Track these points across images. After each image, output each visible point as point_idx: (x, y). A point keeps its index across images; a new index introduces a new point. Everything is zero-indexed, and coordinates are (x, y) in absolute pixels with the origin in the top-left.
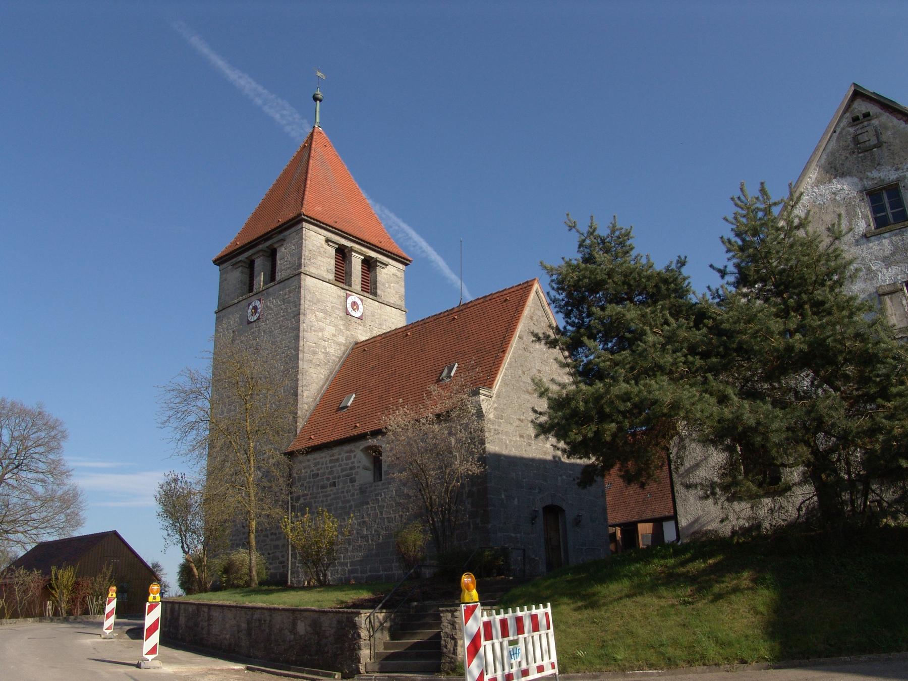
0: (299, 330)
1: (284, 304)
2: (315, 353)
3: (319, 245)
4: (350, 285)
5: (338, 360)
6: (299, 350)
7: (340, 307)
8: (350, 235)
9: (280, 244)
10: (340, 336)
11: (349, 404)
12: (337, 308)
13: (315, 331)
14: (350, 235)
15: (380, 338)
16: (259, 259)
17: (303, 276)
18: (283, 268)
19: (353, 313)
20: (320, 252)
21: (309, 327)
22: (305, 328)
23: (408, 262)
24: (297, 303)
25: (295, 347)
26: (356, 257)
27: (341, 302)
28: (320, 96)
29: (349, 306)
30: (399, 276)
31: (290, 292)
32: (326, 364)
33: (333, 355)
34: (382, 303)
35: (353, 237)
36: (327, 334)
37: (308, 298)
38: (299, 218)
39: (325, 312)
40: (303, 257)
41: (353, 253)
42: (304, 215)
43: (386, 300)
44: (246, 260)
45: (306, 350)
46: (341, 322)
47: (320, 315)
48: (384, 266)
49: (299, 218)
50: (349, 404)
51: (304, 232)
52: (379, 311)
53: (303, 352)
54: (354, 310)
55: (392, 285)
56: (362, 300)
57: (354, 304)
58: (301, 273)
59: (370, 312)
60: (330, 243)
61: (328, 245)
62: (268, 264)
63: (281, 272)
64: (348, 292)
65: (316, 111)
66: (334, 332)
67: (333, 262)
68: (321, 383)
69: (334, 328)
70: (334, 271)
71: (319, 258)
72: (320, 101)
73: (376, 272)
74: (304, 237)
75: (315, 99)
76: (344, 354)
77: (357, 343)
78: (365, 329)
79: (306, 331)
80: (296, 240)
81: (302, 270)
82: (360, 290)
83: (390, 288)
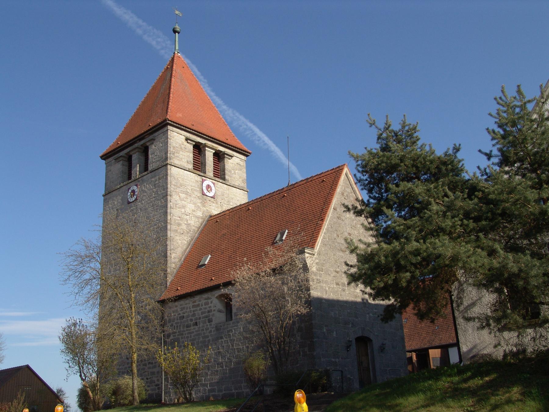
1: (155, 188)
2: (179, 225)
3: (181, 142)
4: (205, 173)
5: (197, 229)
6: (167, 223)
7: (198, 189)
8: (204, 135)
10: (198, 212)
11: (206, 263)
13: (179, 208)
14: (204, 135)
15: (228, 212)
16: (135, 155)
17: (169, 167)
18: (154, 161)
21: (175, 205)
22: (172, 205)
23: (248, 154)
27: (198, 186)
30: (242, 165)
31: (159, 179)
32: (188, 233)
33: (193, 226)
35: (206, 136)
36: (188, 210)
37: (173, 183)
39: (187, 193)
40: (169, 152)
41: (207, 148)
42: (169, 120)
43: (233, 183)
45: (173, 222)
46: (199, 201)
47: (183, 196)
48: (230, 158)
50: (206, 263)
51: (169, 133)
52: (227, 192)
55: (237, 172)
56: (214, 184)
58: (168, 164)
60: (189, 141)
61: (188, 142)
62: (143, 159)
64: (204, 178)
65: (175, 41)
66: (193, 208)
68: (185, 247)
70: (192, 162)
71: (181, 153)
72: (179, 33)
73: (224, 162)
75: (175, 31)
76: (201, 224)
77: (211, 216)
78: (217, 205)
79: (172, 208)
80: (163, 139)
81: (169, 162)
83: (235, 174)
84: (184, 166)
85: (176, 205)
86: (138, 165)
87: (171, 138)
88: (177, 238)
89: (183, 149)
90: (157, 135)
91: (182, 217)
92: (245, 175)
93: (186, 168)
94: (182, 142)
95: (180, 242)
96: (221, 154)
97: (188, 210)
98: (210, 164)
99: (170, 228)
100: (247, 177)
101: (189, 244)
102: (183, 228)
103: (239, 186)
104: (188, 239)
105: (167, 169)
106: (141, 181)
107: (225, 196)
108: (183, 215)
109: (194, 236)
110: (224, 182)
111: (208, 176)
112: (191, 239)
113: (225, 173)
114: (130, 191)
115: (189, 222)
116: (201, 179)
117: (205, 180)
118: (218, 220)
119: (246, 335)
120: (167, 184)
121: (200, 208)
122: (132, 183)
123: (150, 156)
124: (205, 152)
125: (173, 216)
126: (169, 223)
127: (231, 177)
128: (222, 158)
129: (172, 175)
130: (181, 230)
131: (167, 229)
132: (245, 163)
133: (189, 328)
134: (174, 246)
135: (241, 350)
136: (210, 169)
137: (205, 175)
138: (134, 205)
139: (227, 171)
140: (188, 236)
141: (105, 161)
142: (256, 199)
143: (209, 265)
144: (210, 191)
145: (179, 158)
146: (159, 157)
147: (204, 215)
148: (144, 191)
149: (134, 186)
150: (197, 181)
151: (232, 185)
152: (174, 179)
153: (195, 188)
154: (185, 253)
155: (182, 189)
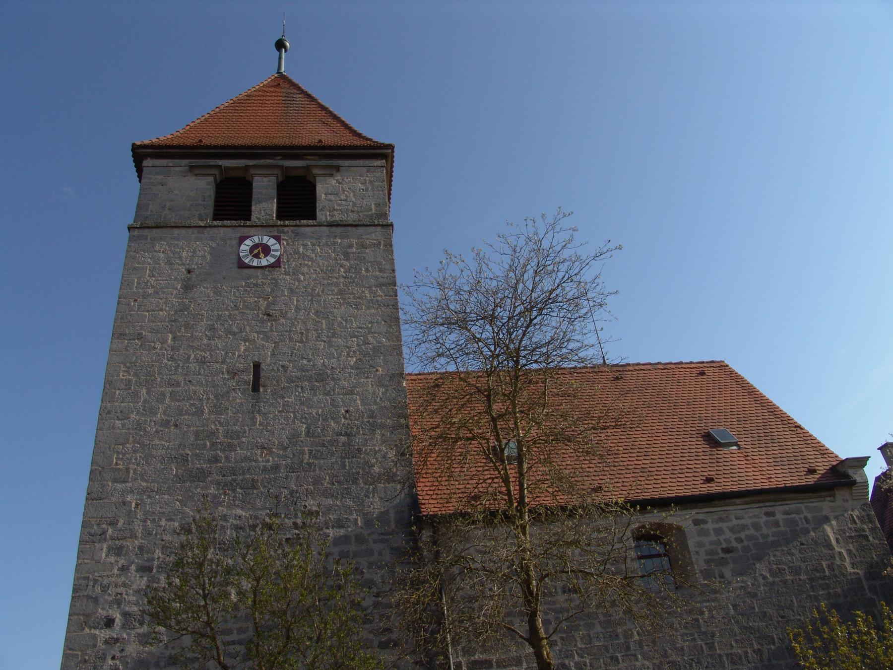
119: (748, 623)
133: (753, 520)
135: (740, 659)
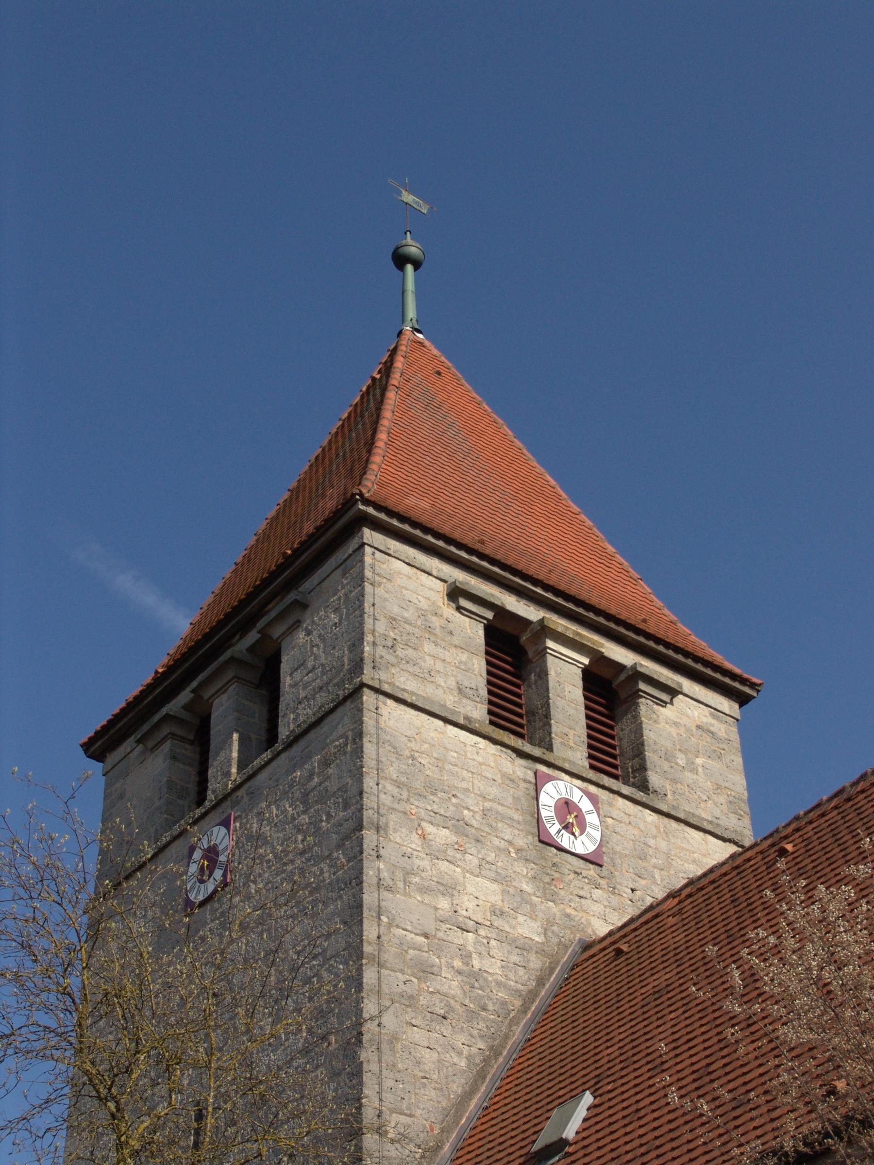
0: (360, 883)
1: (304, 812)
2: (425, 971)
3: (424, 605)
4: (550, 748)
5: (518, 1003)
6: (360, 955)
7: (517, 816)
8: (536, 582)
9: (290, 621)
10: (521, 919)
11: (570, 1133)
12: (503, 818)
13: (423, 890)
14: (536, 582)
15: (672, 902)
16: (224, 697)
17: (368, 697)
18: (302, 694)
19: (565, 840)
20: (429, 629)
21: (399, 875)
22: (385, 875)
23: (747, 690)
24: (354, 791)
25: (348, 946)
26: (561, 657)
27: (516, 799)
28: (413, 250)
29: (547, 813)
30: (722, 734)
31: (326, 763)
32: (472, 1015)
33: (499, 984)
34: (668, 816)
35: (547, 587)
36: (468, 906)
37: (392, 771)
38: (351, 514)
39: (460, 826)
40: (369, 638)
41: (550, 644)
42: (367, 502)
43: (684, 809)
44: (184, 715)
45: (390, 955)
46: (521, 868)
47: (441, 835)
48: (665, 697)
49: (351, 514)
50: (570, 1133)
51: (368, 559)
52: (663, 845)
53: (380, 965)
54: (567, 827)
55: (699, 761)
56: (593, 799)
57: (566, 807)
58: (363, 685)
59: (630, 845)
60: (463, 602)
61: (459, 608)
62: (259, 711)
63: (348, 928)
64: (543, 768)
65: (403, 292)
66: (496, 899)
67: (479, 665)
68: (457, 1088)
69: (495, 887)
70: (484, 692)
71: (428, 647)
72: (417, 265)
73: (636, 717)
74: (368, 573)
75: (400, 260)
76: (541, 982)
77: (587, 946)
78: (615, 900)
79: (389, 889)
80: (341, 593)
81: (368, 675)
82: (587, 764)
83: (694, 771)
84: (444, 706)
85: (408, 873)
86: (235, 736)
87: (377, 578)
88: (417, 1035)
89: (438, 631)
90: (316, 582)
91: (440, 935)
92: (738, 783)
93: (454, 712)
94: (434, 603)
95: (429, 1057)
96: (623, 677)
97: (471, 905)
98: (572, 712)
99: (375, 981)
100: (750, 787)
101: (481, 1075)
102: (444, 989)
103: (718, 825)
104: (474, 1050)
105: (361, 710)
106: (246, 799)
107: (654, 861)
108: (444, 927)
109: (506, 1037)
110: (640, 795)
111: (564, 760)
112: (491, 1048)
113: (643, 759)
114: (197, 855)
115: (476, 963)
116: (530, 776)
117: (551, 778)
118: (625, 948)
120: (361, 774)
121: (533, 906)
122: (207, 819)
123: (286, 681)
124: (545, 661)
125: (390, 925)
126: (372, 958)
127: (674, 781)
128: (625, 701)
129: (383, 736)
130: (436, 998)
131: (360, 987)
132: (734, 729)
134: (398, 1076)
136: (571, 733)
137: (548, 757)
138: (214, 911)
139: (655, 751)
140: (475, 1032)
141: (101, 764)
142: (818, 806)
143: (586, 1142)
144: (576, 830)
145: (416, 670)
146: (324, 673)
147: (555, 940)
148: (259, 839)
149: (216, 829)
150: (512, 780)
151: (682, 816)
152: (393, 757)
153: (500, 808)
154: (457, 1122)
155: (435, 807)
